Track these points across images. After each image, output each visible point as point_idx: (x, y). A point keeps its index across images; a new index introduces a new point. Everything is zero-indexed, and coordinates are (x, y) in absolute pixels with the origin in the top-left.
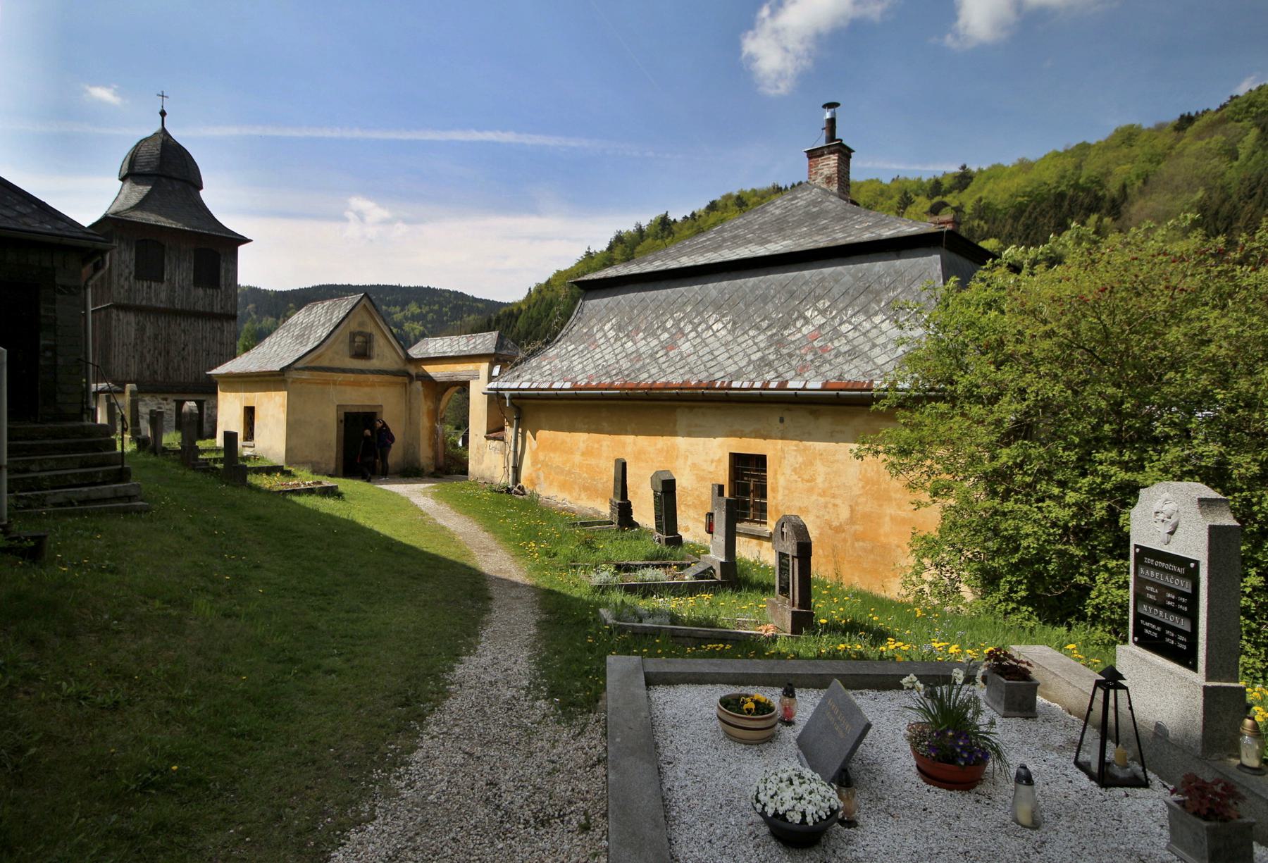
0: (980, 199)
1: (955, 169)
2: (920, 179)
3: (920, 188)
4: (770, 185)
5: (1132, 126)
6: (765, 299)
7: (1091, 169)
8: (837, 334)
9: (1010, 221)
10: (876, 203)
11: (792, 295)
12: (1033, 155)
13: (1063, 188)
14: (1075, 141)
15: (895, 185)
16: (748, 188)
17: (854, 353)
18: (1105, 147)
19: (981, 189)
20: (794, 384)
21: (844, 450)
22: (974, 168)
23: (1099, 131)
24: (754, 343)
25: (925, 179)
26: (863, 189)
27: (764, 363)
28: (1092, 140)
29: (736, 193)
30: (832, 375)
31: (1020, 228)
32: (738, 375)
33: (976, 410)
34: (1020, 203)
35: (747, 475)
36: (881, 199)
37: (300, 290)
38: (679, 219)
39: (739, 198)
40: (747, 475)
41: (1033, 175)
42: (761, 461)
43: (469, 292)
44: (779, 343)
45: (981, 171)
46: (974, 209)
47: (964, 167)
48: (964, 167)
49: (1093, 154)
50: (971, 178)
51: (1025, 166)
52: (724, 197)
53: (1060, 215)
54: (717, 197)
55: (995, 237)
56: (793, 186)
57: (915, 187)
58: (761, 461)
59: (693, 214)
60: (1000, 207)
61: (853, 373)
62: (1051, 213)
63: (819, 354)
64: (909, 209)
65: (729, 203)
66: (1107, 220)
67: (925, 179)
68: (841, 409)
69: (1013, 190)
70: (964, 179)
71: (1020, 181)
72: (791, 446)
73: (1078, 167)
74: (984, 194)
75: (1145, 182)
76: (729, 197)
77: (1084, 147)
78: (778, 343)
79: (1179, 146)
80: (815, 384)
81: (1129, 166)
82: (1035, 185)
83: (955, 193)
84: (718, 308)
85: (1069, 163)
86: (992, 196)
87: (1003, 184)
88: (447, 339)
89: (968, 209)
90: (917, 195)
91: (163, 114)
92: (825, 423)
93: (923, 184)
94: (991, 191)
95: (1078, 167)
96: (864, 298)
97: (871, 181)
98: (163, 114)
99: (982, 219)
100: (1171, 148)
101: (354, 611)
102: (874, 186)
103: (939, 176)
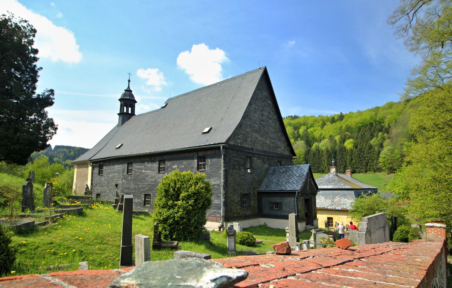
0: (347, 125)
1: (339, 113)
2: (327, 116)
3: (328, 119)
5: (391, 102)
6: (329, 195)
7: (380, 116)
8: (341, 201)
9: (356, 133)
10: (314, 124)
11: (334, 194)
12: (363, 108)
13: (372, 121)
14: (374, 106)
15: (319, 118)
17: (344, 204)
18: (384, 108)
19: (347, 121)
20: (337, 208)
21: (346, 217)
22: (344, 113)
23: (381, 103)
25: (329, 116)
26: (310, 119)
27: (331, 205)
28: (380, 105)
30: (342, 207)
31: (360, 136)
32: (328, 206)
33: (360, 213)
34: (359, 126)
35: (330, 219)
36: (315, 123)
40: (330, 219)
41: (363, 117)
42: (332, 218)
45: (346, 114)
46: (345, 128)
47: (341, 113)
48: (341, 113)
49: (380, 110)
50: (344, 117)
51: (360, 113)
53: (371, 132)
55: (352, 138)
56: (287, 117)
57: (326, 119)
58: (332, 218)
60: (353, 127)
61: (345, 207)
62: (369, 131)
64: (325, 126)
66: (385, 135)
67: (329, 116)
68: (344, 211)
69: (357, 122)
70: (341, 117)
71: (358, 119)
72: (336, 216)
73: (376, 115)
74: (348, 123)
75: (396, 122)
77: (378, 108)
79: (405, 110)
80: (340, 208)
81: (391, 116)
82: (363, 120)
83: (339, 121)
84: (322, 195)
85: (373, 113)
86: (350, 124)
87: (354, 120)
89: (344, 128)
90: (327, 122)
91: (129, 81)
92: (341, 213)
93: (329, 118)
94: (350, 122)
95: (376, 115)
96: (345, 196)
97: (312, 116)
98: (129, 81)
99: (348, 131)
100: (402, 110)
102: (313, 118)
103: (333, 115)
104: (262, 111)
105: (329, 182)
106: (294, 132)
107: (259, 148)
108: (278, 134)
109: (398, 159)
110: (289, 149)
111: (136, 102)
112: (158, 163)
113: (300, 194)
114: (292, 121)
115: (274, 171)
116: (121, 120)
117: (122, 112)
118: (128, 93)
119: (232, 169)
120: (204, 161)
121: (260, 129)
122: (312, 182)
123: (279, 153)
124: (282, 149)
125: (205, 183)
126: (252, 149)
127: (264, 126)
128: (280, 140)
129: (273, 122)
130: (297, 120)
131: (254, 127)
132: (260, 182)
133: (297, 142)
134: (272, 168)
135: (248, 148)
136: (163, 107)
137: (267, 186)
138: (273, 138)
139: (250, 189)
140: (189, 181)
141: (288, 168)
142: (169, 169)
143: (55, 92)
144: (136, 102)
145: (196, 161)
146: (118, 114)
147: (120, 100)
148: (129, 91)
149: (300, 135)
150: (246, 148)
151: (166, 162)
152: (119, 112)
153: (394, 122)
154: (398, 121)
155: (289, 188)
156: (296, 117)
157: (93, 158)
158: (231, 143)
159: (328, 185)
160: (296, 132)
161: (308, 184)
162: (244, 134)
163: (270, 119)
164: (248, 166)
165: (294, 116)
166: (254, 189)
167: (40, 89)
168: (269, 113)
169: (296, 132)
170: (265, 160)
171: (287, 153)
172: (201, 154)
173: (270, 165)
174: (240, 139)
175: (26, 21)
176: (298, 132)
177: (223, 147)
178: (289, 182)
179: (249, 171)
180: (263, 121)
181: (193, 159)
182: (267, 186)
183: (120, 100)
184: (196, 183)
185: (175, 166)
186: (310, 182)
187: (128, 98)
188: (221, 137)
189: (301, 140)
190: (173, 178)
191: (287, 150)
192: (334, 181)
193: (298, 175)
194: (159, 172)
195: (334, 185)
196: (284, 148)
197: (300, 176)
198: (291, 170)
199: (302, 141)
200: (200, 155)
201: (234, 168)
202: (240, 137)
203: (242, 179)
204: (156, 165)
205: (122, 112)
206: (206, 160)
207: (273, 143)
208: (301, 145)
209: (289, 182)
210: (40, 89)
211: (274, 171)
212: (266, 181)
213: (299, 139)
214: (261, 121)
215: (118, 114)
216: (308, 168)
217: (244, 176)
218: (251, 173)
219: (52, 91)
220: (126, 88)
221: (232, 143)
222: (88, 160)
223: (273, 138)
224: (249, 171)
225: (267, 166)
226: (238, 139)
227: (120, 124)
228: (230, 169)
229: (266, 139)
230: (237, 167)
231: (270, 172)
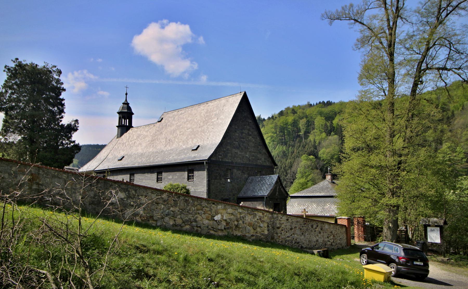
4: (306, 103)
16: (297, 105)
24: (320, 208)
27: (322, 212)
29: (291, 107)
32: (318, 213)
37: (174, 172)
38: (266, 118)
39: (293, 110)
43: (95, 144)
44: (323, 209)
52: (286, 109)
54: (283, 109)
56: (317, 104)
59: (273, 117)
63: (329, 210)
65: (289, 111)
75: (463, 109)
76: (288, 109)
78: (323, 209)
88: (250, 203)
91: (126, 94)
98: (126, 94)
101: (391, 43)
104: (242, 130)
105: (322, 189)
106: (326, 124)
107: (239, 161)
108: (258, 148)
109: (462, 158)
110: (270, 160)
111: (133, 114)
112: (156, 174)
113: (268, 199)
114: (323, 109)
115: (252, 180)
116: (120, 132)
117: (120, 124)
118: (126, 106)
119: (214, 179)
120: (193, 173)
121: (240, 146)
122: (282, 189)
123: (259, 164)
124: (263, 160)
125: (186, 189)
126: (232, 163)
127: (244, 142)
128: (260, 153)
129: (253, 137)
130: (329, 108)
131: (234, 144)
132: (240, 190)
133: (330, 137)
134: (251, 178)
135: (228, 162)
136: (159, 122)
137: (245, 193)
138: (253, 152)
139: (230, 195)
140: (177, 188)
141: (263, 178)
142: (166, 180)
143: (79, 122)
144: (133, 114)
145: (186, 173)
146: (117, 126)
147: (119, 113)
148: (126, 103)
149: (334, 127)
150: (226, 162)
151: (163, 173)
152: (118, 125)
153: (460, 108)
154: (465, 107)
155: (260, 194)
156: (329, 103)
157: (96, 170)
158: (213, 159)
159: (320, 193)
160: (328, 124)
161: (278, 191)
162: (224, 151)
163: (250, 135)
164: (229, 176)
165: (327, 102)
166: (234, 195)
167: (66, 121)
168: (249, 130)
169: (328, 124)
170: (244, 171)
171: (268, 164)
172: (190, 167)
173: (249, 175)
174: (221, 155)
175: (55, 67)
176: (332, 123)
177: (206, 163)
178: (261, 189)
179: (229, 180)
180: (243, 138)
181: (184, 171)
182: (245, 193)
183: (119, 113)
184: (182, 189)
185: (170, 177)
186: (280, 189)
187: (126, 111)
188: (205, 155)
189: (336, 134)
190: (169, 187)
191: (268, 161)
192: (327, 188)
193: (269, 184)
194: (157, 181)
195: (326, 192)
196: (265, 159)
197: (270, 184)
198: (264, 180)
199: (336, 136)
200: (190, 168)
201: (216, 179)
202: (221, 154)
203: (223, 187)
204: (154, 176)
205: (120, 124)
206: (195, 172)
207: (253, 156)
208: (334, 141)
209: (261, 189)
210: (66, 121)
211: (252, 180)
212: (245, 188)
213: (332, 133)
214: (241, 138)
215: (117, 126)
216: (277, 178)
217: (224, 184)
218: (231, 182)
219: (77, 121)
220: (124, 101)
221: (214, 159)
222: (93, 171)
223: (253, 152)
224: (229, 180)
225: (246, 176)
226: (219, 155)
227: (119, 136)
228: (212, 179)
229: (246, 153)
230: (218, 178)
231: (249, 181)
